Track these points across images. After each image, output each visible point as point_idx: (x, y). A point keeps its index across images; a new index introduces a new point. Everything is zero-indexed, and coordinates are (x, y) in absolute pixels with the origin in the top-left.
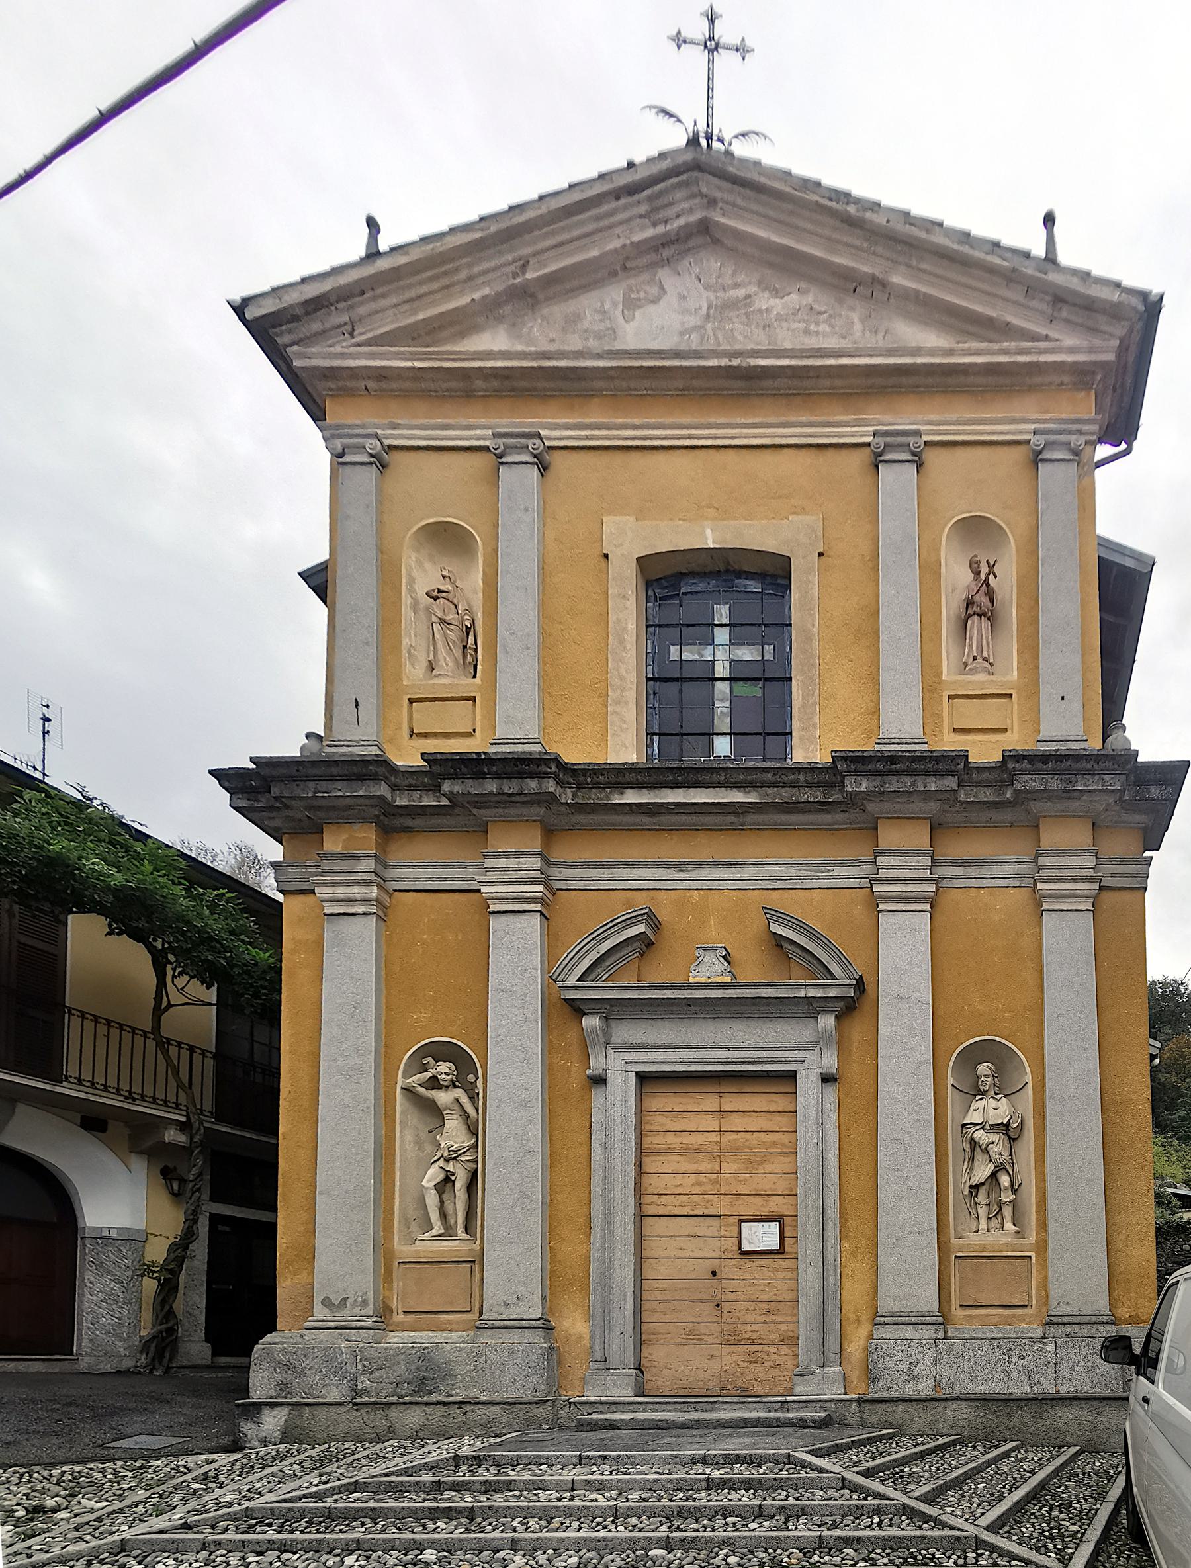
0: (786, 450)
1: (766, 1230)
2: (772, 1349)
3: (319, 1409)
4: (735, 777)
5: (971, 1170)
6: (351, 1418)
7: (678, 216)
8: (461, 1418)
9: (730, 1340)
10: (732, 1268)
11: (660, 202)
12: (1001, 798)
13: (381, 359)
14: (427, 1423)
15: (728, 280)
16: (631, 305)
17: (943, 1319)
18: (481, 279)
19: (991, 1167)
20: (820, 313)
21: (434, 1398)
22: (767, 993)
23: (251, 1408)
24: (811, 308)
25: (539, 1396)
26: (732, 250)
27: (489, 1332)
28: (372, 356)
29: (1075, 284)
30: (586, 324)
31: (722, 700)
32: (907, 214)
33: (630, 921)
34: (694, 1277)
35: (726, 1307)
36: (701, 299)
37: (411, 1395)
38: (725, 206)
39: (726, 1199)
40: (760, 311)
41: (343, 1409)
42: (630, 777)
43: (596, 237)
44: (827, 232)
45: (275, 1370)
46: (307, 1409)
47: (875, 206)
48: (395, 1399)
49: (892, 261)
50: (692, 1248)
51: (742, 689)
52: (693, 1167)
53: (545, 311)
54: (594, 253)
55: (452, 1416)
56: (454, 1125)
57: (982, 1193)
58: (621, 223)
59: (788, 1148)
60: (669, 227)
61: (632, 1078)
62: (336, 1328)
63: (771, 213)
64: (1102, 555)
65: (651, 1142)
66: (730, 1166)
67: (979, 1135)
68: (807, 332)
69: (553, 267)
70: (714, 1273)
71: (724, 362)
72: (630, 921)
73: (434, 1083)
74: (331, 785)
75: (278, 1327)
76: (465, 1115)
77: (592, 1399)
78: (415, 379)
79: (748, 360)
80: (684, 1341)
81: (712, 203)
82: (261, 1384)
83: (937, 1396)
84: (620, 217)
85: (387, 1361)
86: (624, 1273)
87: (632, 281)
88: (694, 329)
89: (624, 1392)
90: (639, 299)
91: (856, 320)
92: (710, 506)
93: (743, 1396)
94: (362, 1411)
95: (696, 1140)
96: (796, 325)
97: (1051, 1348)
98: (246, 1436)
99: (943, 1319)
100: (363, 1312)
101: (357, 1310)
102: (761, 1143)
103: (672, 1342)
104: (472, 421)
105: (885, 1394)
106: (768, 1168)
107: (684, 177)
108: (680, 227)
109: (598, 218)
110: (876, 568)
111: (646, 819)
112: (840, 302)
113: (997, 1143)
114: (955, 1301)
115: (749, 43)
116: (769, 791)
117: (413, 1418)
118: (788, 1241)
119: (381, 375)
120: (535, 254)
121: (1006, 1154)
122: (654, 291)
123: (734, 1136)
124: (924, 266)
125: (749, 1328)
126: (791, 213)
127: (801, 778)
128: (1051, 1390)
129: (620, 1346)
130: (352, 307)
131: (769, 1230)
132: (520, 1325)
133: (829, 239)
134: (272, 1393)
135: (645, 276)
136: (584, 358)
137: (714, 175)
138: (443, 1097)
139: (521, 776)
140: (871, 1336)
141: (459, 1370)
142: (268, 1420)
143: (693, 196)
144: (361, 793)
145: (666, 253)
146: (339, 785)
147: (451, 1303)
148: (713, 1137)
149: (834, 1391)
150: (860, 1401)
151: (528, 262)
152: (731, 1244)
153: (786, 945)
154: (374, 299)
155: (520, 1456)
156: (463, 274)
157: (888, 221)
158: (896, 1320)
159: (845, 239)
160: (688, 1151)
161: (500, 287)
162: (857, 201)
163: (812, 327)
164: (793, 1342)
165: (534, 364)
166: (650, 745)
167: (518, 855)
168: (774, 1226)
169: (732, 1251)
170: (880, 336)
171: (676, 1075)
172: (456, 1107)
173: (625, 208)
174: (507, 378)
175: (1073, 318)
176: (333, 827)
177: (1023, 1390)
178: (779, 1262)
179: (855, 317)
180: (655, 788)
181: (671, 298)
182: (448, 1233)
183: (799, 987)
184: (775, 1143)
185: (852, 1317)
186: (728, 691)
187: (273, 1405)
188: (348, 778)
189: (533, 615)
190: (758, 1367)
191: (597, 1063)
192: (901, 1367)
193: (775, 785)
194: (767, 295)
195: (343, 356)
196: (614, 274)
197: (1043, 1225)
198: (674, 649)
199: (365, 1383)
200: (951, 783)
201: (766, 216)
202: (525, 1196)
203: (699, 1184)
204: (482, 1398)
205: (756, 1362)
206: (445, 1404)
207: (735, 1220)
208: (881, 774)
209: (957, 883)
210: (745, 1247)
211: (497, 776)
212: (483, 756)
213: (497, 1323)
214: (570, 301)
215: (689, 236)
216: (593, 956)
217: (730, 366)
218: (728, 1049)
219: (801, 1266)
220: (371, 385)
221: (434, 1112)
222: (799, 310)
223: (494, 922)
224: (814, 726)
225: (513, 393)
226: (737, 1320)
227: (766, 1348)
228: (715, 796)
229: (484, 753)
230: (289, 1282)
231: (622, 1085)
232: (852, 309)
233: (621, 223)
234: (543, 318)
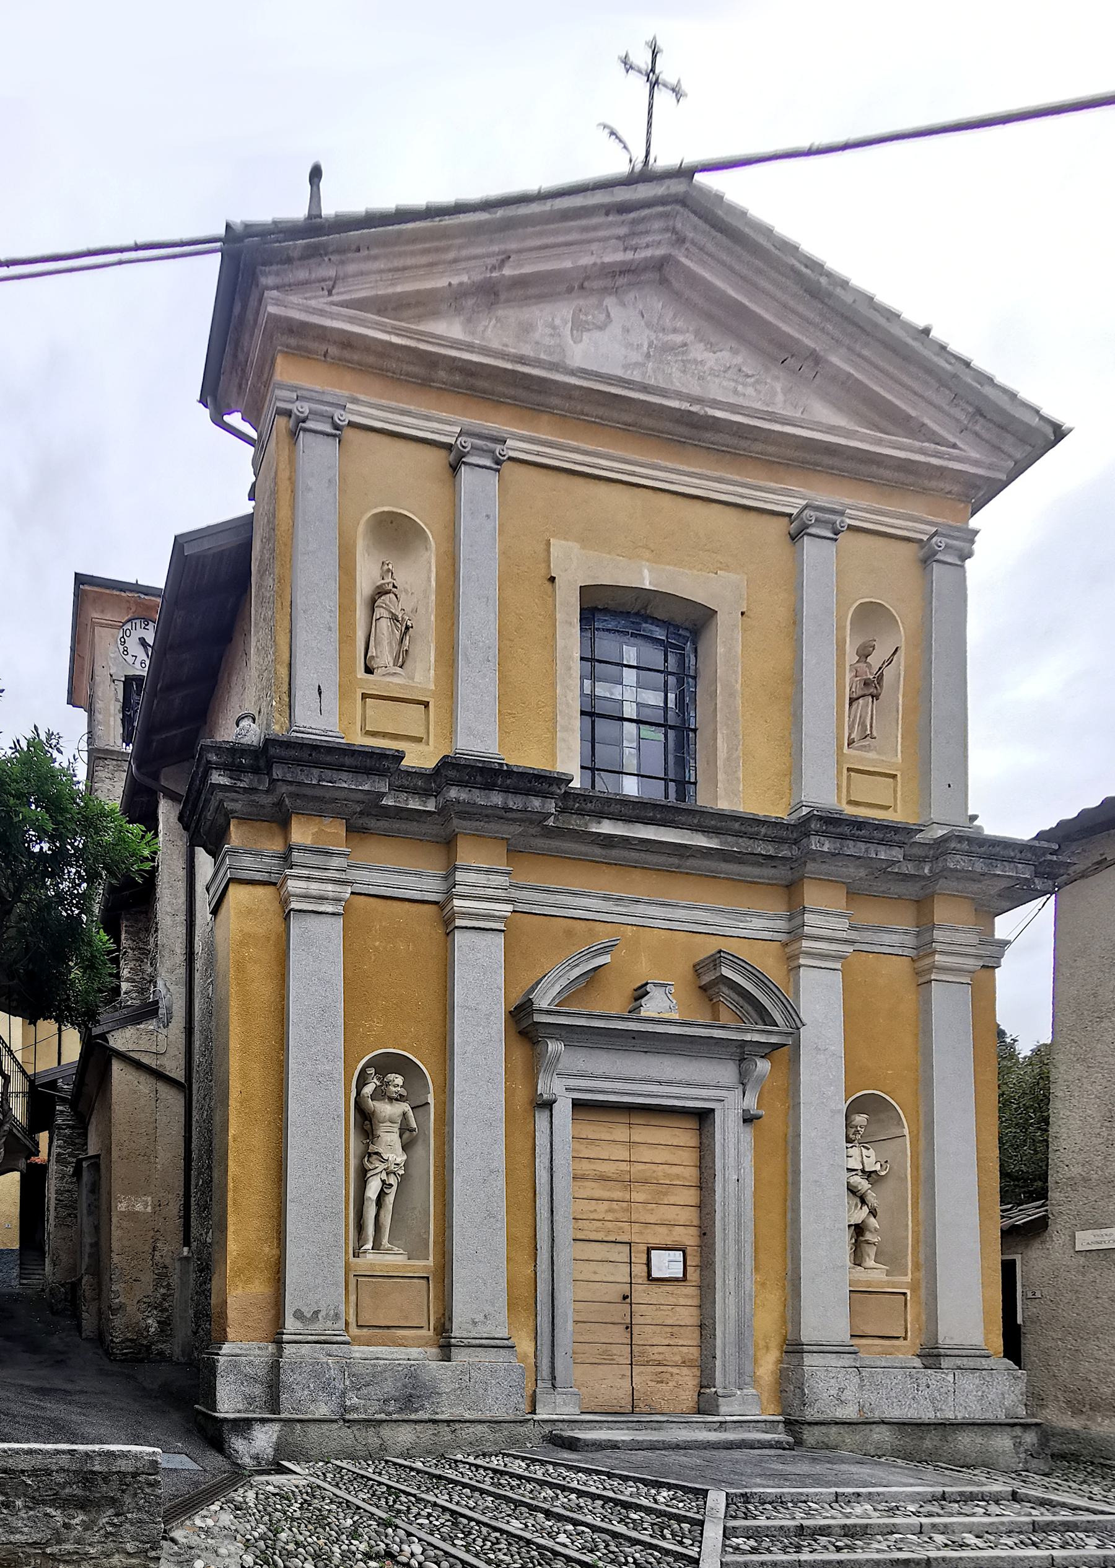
0: (714, 505)
1: (671, 1259)
2: (675, 1370)
3: (312, 1426)
7: (647, 246)
8: (449, 1437)
10: (641, 1293)
11: (641, 228)
12: (920, 873)
13: (360, 325)
14: (417, 1440)
15: (667, 321)
16: (579, 326)
18: (463, 265)
20: (748, 376)
22: (718, 1034)
23: (241, 1424)
24: (740, 370)
26: (677, 295)
28: (352, 320)
29: (1004, 402)
30: (537, 336)
31: (630, 741)
32: (870, 299)
33: (602, 951)
34: (606, 1300)
36: (643, 337)
37: (398, 1412)
38: (693, 249)
40: (695, 362)
41: (335, 1426)
42: (615, 808)
43: (573, 248)
44: (784, 298)
45: (242, 1383)
46: (298, 1426)
47: (844, 284)
48: (383, 1416)
49: (837, 341)
50: (603, 1272)
51: (647, 732)
52: (606, 1194)
53: (500, 313)
54: (568, 264)
55: (441, 1434)
58: (599, 240)
59: (690, 1181)
60: (637, 256)
62: (320, 1343)
63: (737, 267)
66: (639, 1195)
69: (527, 269)
71: (685, 406)
72: (602, 951)
74: (335, 775)
75: (230, 1337)
78: (381, 355)
79: (707, 409)
80: (597, 1361)
81: (681, 240)
84: (601, 234)
85: (375, 1377)
87: (581, 302)
88: (636, 364)
90: (586, 322)
91: (779, 390)
92: (646, 547)
94: (354, 1428)
95: (608, 1169)
96: (725, 383)
97: (950, 1378)
98: (238, 1452)
100: (336, 1326)
101: (329, 1324)
102: (667, 1175)
103: (587, 1361)
104: (434, 413)
106: (672, 1199)
107: (668, 208)
108: (646, 259)
109: (585, 229)
111: (598, 850)
112: (767, 370)
115: (685, 87)
116: (730, 839)
117: (404, 1436)
119: (348, 341)
120: (519, 251)
123: (641, 1167)
124: (866, 352)
125: (656, 1349)
126: (759, 272)
127: (763, 830)
128: (950, 1415)
130: (342, 262)
131: (674, 1259)
133: (785, 306)
134: (240, 1406)
135: (593, 300)
136: (557, 371)
137: (695, 213)
139: (528, 793)
141: (445, 1388)
142: (259, 1436)
143: (666, 230)
144: (366, 788)
145: (621, 281)
146: (344, 776)
147: (406, 1318)
148: (624, 1166)
151: (509, 257)
154: (368, 258)
155: (783, 1494)
156: (451, 255)
157: (854, 301)
159: (801, 308)
160: (603, 1178)
161: (478, 277)
162: (829, 275)
163: (740, 388)
165: (509, 366)
167: (488, 871)
169: (641, 1277)
171: (596, 1103)
173: (611, 225)
174: (472, 374)
175: (983, 433)
176: (303, 819)
177: (928, 1415)
179: (778, 386)
180: (630, 821)
181: (615, 329)
184: (678, 1177)
185: (762, 1343)
188: (355, 770)
189: (494, 628)
192: (832, 1392)
193: (738, 834)
194: (702, 346)
195: (321, 313)
196: (570, 290)
199: (353, 1400)
200: (897, 854)
201: (731, 269)
202: (491, 1215)
203: (610, 1211)
204: (468, 1416)
205: (662, 1382)
206: (435, 1422)
208: (843, 837)
211: (506, 790)
212: (505, 768)
215: (645, 269)
217: (689, 411)
218: (660, 1083)
220: (333, 350)
222: (730, 367)
223: (458, 935)
224: (738, 779)
225: (468, 392)
226: (646, 1343)
227: (670, 1369)
228: (682, 837)
229: (507, 765)
230: (239, 1291)
232: (777, 378)
233: (599, 240)
234: (498, 320)
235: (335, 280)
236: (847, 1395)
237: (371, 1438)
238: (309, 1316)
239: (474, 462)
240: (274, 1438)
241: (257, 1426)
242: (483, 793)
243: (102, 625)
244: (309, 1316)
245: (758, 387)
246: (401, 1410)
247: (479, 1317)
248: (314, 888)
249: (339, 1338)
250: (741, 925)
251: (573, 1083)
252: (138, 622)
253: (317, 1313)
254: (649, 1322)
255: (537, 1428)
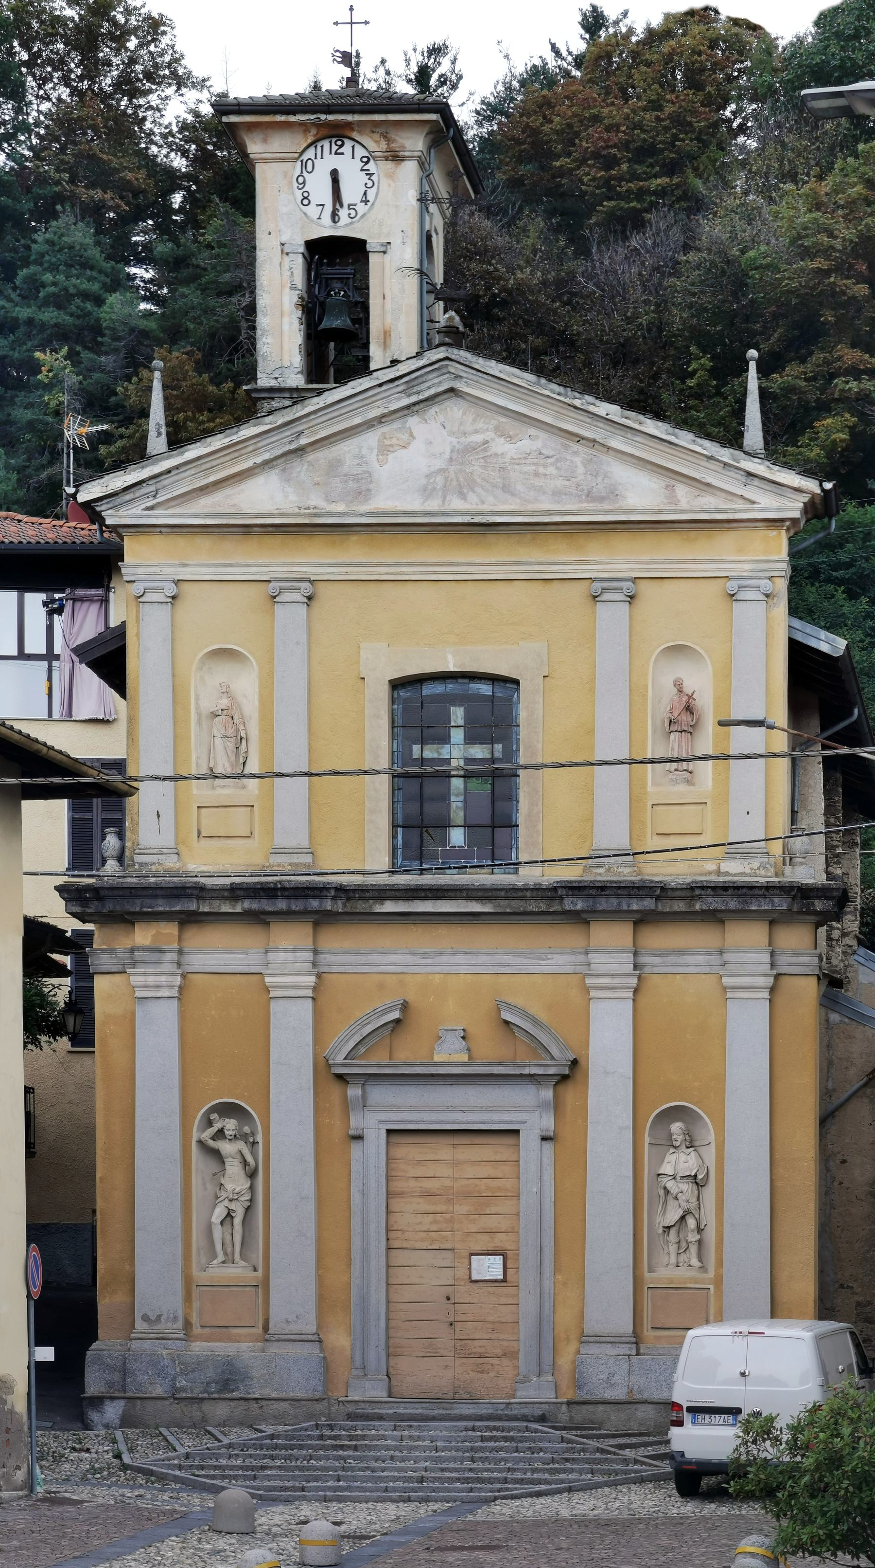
2: (496, 1361)
3: (149, 1402)
4: (474, 894)
5: (665, 1212)
6: (176, 1410)
9: (462, 1353)
10: (463, 1294)
12: (691, 910)
15: (469, 428)
16: (385, 450)
17: (637, 1339)
19: (680, 1213)
21: (236, 1394)
25: (318, 1395)
27: (277, 1344)
30: (345, 469)
31: (457, 795)
35: (458, 1326)
39: (458, 1236)
40: (496, 455)
41: (167, 1403)
46: (139, 1402)
48: (206, 1395)
51: (474, 784)
52: (432, 1208)
56: (234, 1168)
57: (673, 1232)
61: (383, 1134)
64: (799, 637)
65: (399, 1186)
66: (461, 1208)
67: (671, 1185)
68: (536, 474)
70: (448, 1298)
73: (220, 1134)
76: (245, 1163)
77: (356, 1398)
81: (458, 377)
82: (93, 1384)
83: (630, 1399)
86: (377, 1298)
88: (441, 471)
89: (380, 1394)
90: (391, 445)
91: (579, 464)
93: (473, 1400)
96: (526, 469)
99: (637, 1339)
100: (175, 1326)
105: (589, 1397)
106: (494, 1209)
110: (592, 690)
113: (687, 1187)
114: (647, 1324)
116: (502, 903)
117: (221, 1410)
118: (510, 1272)
121: (694, 1200)
122: (405, 437)
125: (477, 1343)
129: (375, 1356)
132: (300, 1339)
138: (226, 1147)
139: (306, 897)
140: (578, 1352)
141: (256, 1373)
146: (160, 901)
148: (448, 1183)
149: (549, 1396)
150: (569, 1403)
152: (462, 1273)
153: (516, 1030)
156: (250, 448)
158: (599, 1339)
160: (427, 1194)
163: (541, 470)
164: (512, 1356)
166: (394, 836)
167: (294, 950)
168: (499, 1260)
170: (600, 479)
172: (239, 1156)
178: (502, 1289)
179: (578, 460)
181: (418, 445)
182: (229, 1260)
183: (524, 1066)
186: (462, 786)
187: (112, 1399)
190: (484, 1376)
191: (356, 1122)
192: (602, 1376)
194: (502, 440)
197: (720, 1263)
198: (416, 749)
199: (182, 1382)
203: (435, 1222)
204: (274, 1395)
205: (482, 1372)
207: (466, 1253)
208: (595, 896)
209: (656, 970)
210: (474, 1277)
213: (283, 1337)
214: (299, 313)
216: (357, 1038)
219: (522, 1294)
221: (217, 1155)
223: (273, 1004)
227: (491, 1361)
230: (107, 1301)
231: (376, 1139)
232: (575, 453)
234: (310, 464)
235: (157, 491)
236: (617, 1379)
237: (194, 1412)
238: (153, 1319)
239: (288, 600)
240: (120, 1412)
241: (107, 1403)
242: (270, 901)
243: (266, 161)
244: (153, 1319)
245: (559, 464)
246: (220, 1391)
247: (291, 1318)
248: (151, 980)
249: (174, 1336)
250: (542, 962)
251: (383, 1116)
252: (326, 144)
253: (159, 1316)
254: (471, 1319)
255: (341, 1407)
